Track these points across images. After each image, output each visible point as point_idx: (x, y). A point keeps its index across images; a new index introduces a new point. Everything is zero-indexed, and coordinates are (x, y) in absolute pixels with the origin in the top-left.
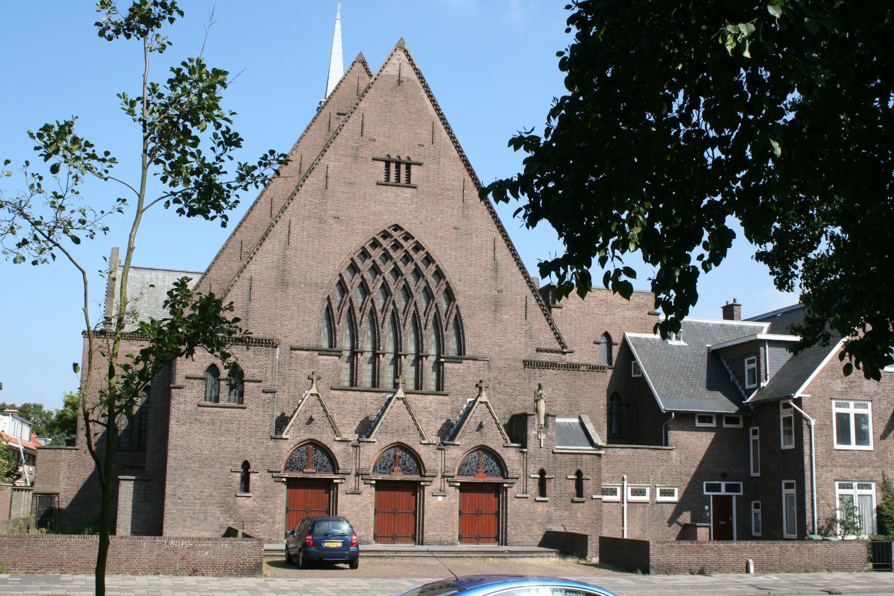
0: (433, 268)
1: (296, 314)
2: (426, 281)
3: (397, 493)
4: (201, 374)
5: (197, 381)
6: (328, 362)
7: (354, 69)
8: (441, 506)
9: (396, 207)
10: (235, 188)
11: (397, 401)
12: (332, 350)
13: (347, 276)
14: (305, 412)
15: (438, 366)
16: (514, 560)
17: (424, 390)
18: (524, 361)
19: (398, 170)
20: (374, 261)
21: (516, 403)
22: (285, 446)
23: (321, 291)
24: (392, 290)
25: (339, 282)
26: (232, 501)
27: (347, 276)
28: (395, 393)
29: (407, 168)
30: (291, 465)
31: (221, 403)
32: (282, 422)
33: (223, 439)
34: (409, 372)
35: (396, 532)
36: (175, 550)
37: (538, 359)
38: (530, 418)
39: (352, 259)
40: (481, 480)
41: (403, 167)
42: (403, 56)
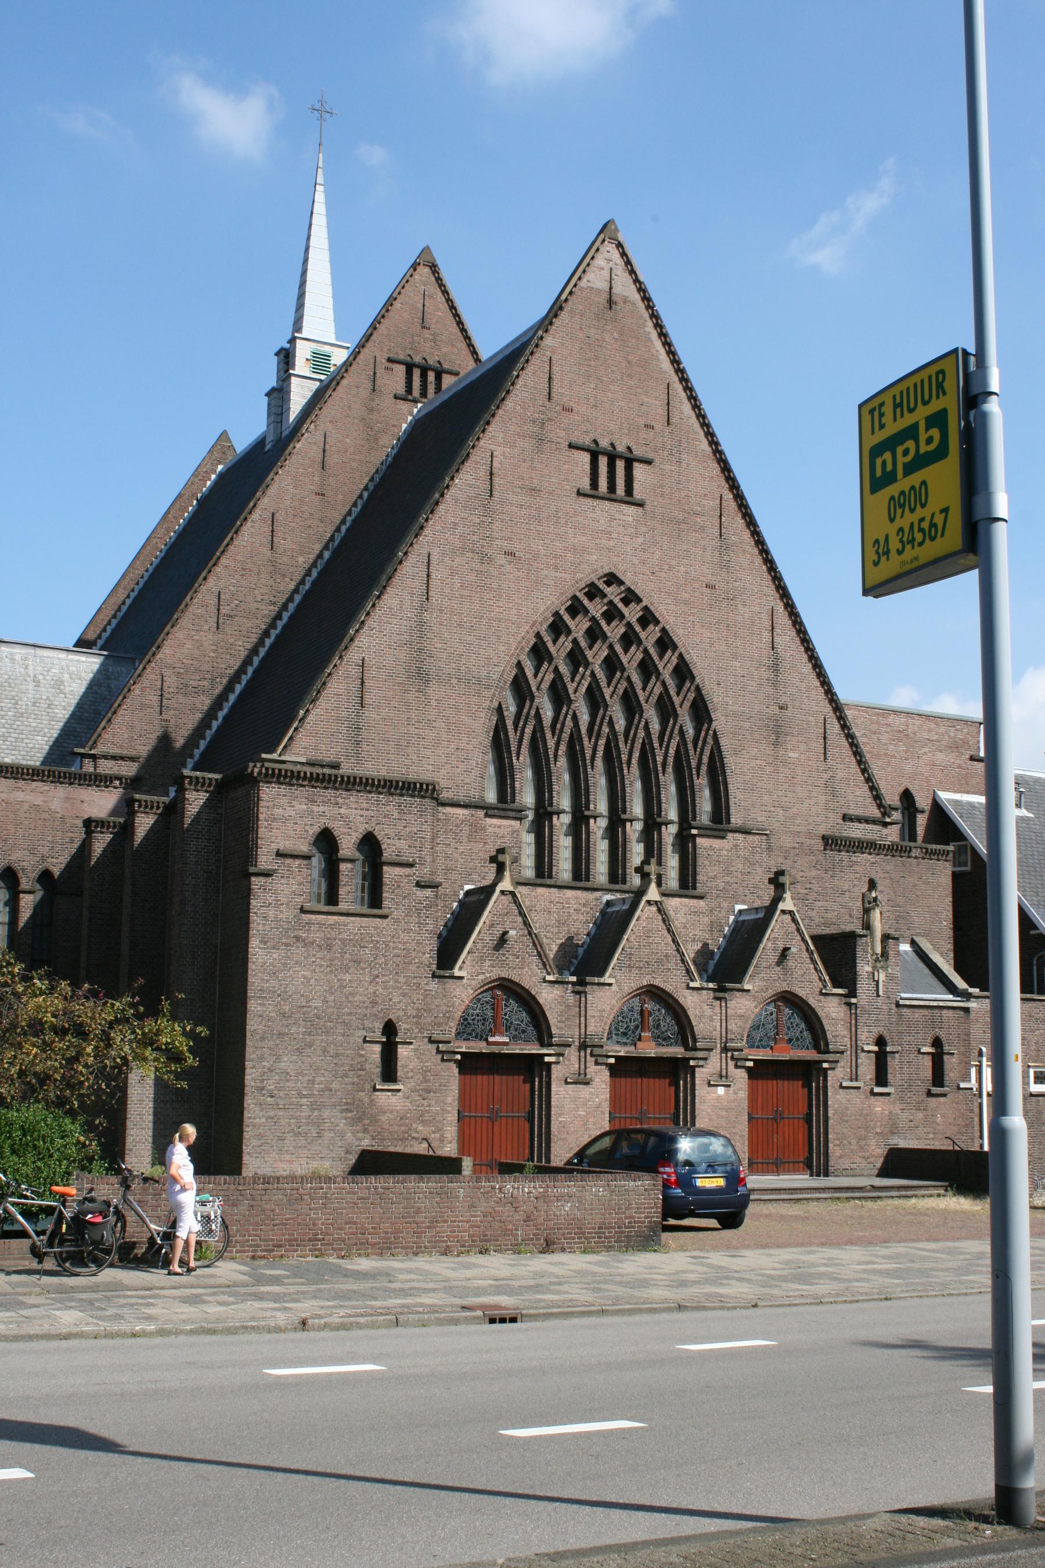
1: (444, 736)
3: (645, 1080)
4: (304, 848)
5: (298, 862)
9: (606, 540)
11: (647, 908)
12: (505, 803)
14: (492, 926)
15: (684, 841)
18: (824, 838)
19: (612, 471)
21: (813, 914)
22: (458, 992)
23: (488, 694)
25: (516, 678)
26: (366, 1100)
30: (466, 1028)
31: (343, 906)
33: (348, 977)
38: (861, 941)
39: (538, 635)
40: (786, 1057)
41: (620, 465)
42: (615, 255)
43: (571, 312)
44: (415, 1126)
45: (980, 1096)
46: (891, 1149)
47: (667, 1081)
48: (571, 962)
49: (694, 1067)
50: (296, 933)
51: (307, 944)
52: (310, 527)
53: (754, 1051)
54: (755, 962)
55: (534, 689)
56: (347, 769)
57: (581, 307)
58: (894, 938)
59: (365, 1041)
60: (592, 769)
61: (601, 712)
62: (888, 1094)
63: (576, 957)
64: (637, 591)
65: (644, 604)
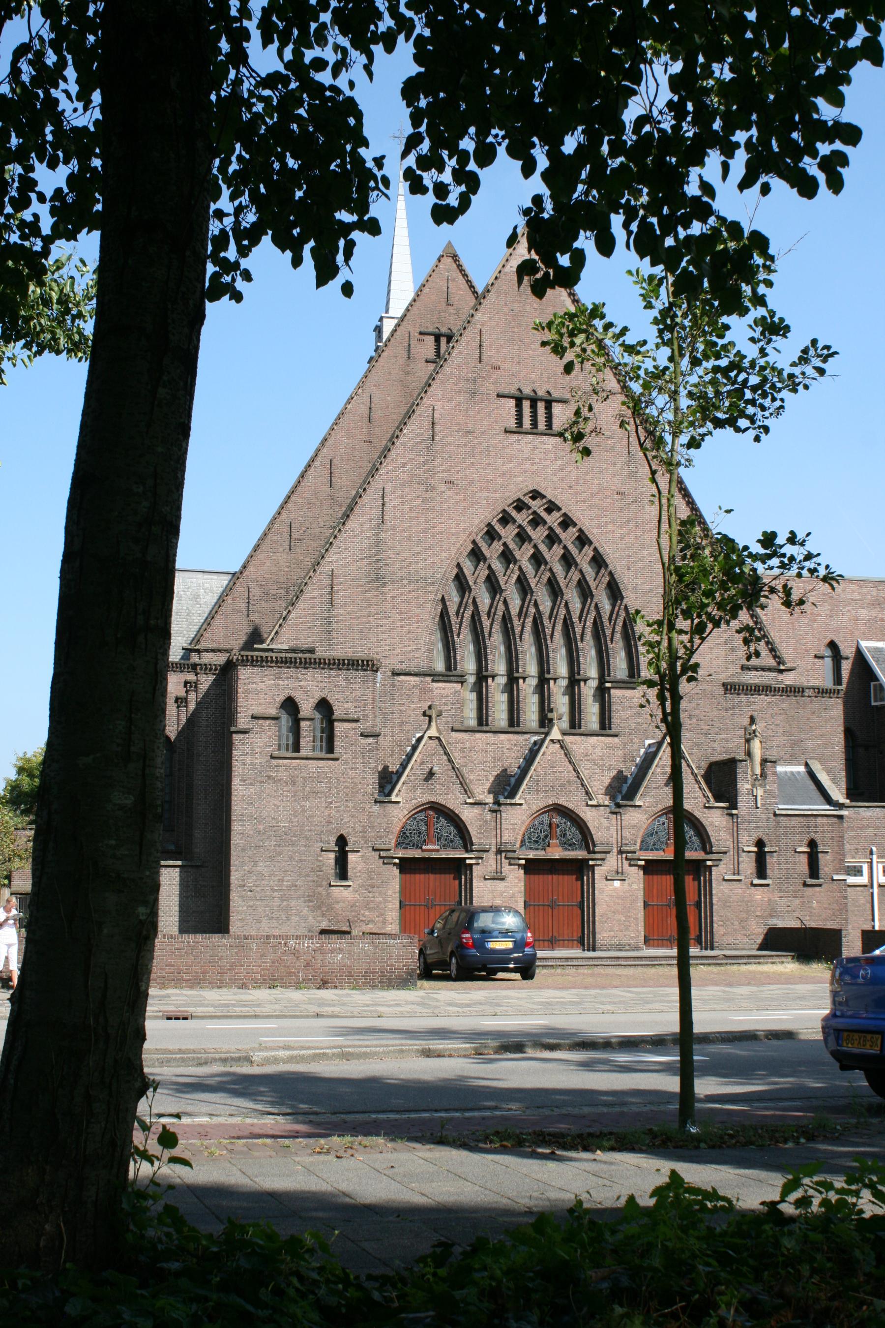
0: (589, 552)
2: (581, 571)
3: (555, 877)
4: (273, 711)
5: (268, 722)
6: (445, 692)
7: (441, 266)
8: (619, 896)
10: (780, 390)
11: (552, 745)
13: (468, 567)
14: (422, 763)
15: (602, 693)
16: (735, 967)
17: (583, 729)
18: (724, 684)
20: (505, 544)
21: (716, 745)
22: (395, 813)
23: (434, 590)
24: (533, 585)
26: (324, 893)
27: (468, 567)
28: (547, 734)
29: (546, 408)
30: (404, 839)
31: (303, 753)
32: (387, 781)
33: (308, 804)
34: (561, 703)
35: (555, 934)
36: (296, 953)
37: (743, 681)
38: (740, 766)
39: (474, 542)
41: (541, 406)
43: (497, 292)
44: (362, 912)
45: (872, 887)
46: (770, 929)
47: (574, 877)
48: (505, 789)
49: (593, 866)
50: (267, 773)
51: (277, 781)
52: (360, 467)
53: (642, 852)
54: (645, 784)
55: (471, 583)
56: (320, 653)
57: (505, 288)
58: (771, 762)
59: (322, 851)
60: (521, 641)
61: (529, 596)
62: (768, 885)
63: (509, 785)
64: (556, 502)
65: (563, 511)
